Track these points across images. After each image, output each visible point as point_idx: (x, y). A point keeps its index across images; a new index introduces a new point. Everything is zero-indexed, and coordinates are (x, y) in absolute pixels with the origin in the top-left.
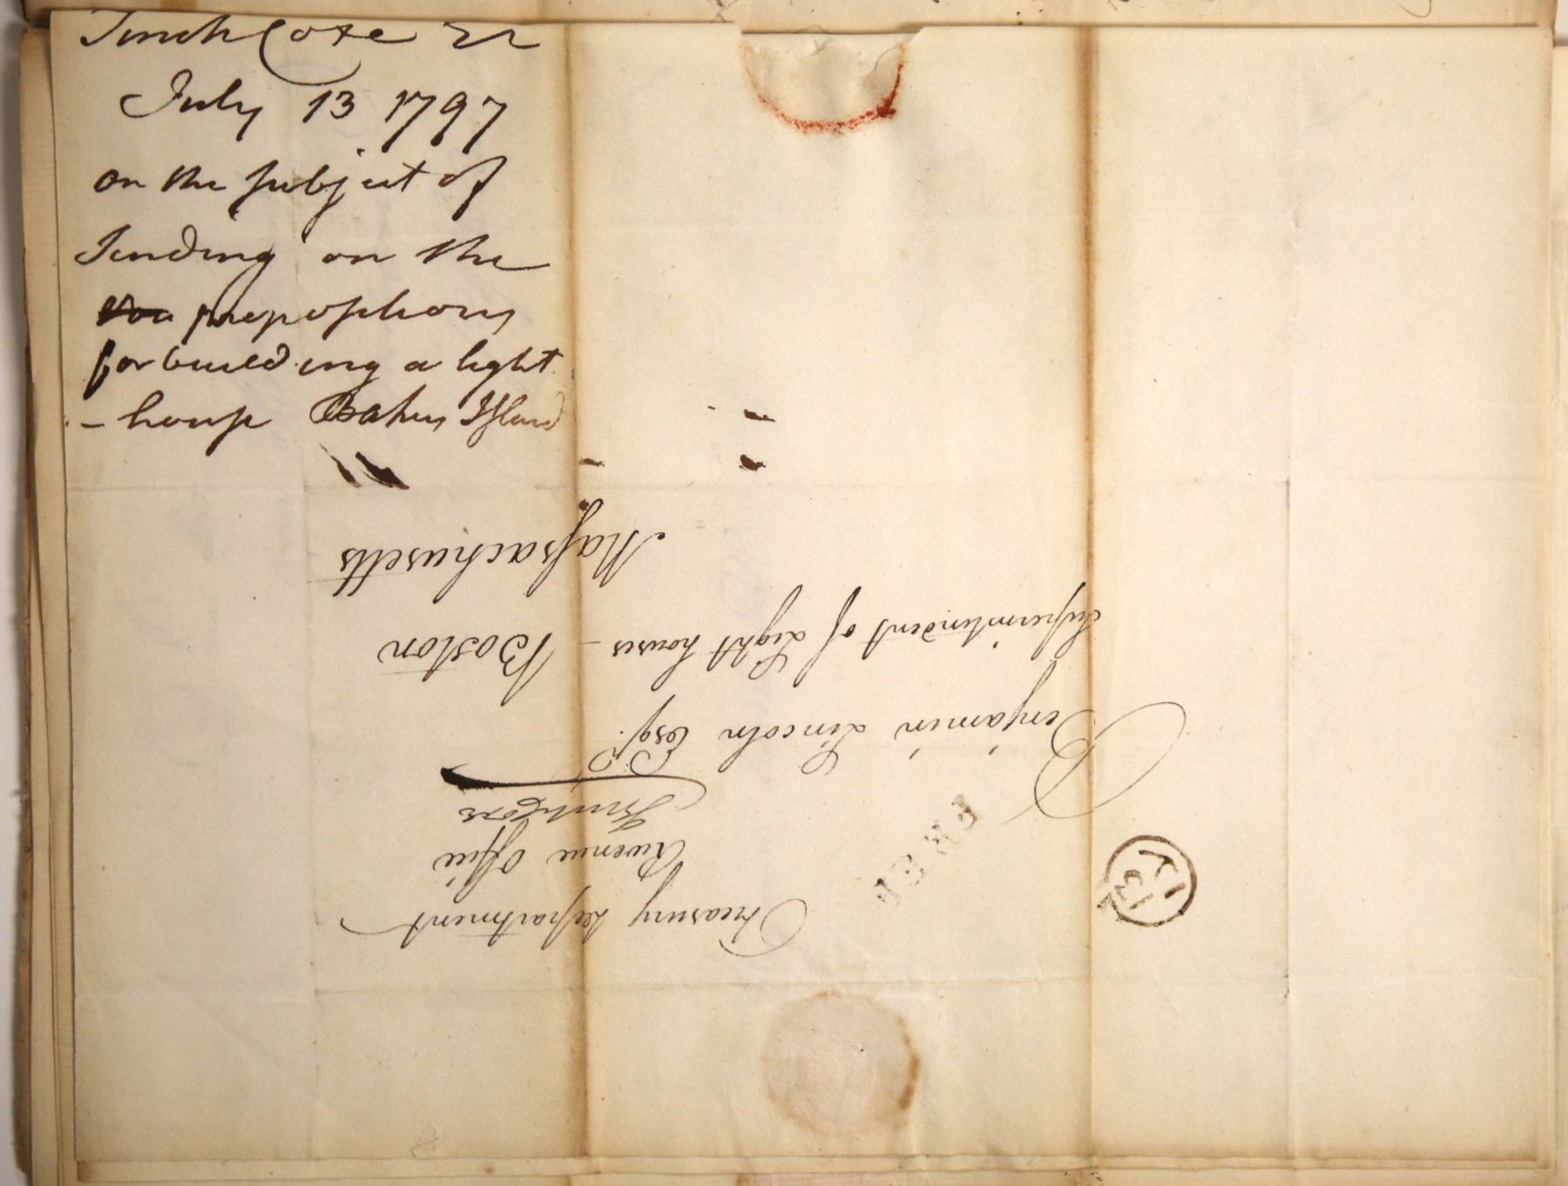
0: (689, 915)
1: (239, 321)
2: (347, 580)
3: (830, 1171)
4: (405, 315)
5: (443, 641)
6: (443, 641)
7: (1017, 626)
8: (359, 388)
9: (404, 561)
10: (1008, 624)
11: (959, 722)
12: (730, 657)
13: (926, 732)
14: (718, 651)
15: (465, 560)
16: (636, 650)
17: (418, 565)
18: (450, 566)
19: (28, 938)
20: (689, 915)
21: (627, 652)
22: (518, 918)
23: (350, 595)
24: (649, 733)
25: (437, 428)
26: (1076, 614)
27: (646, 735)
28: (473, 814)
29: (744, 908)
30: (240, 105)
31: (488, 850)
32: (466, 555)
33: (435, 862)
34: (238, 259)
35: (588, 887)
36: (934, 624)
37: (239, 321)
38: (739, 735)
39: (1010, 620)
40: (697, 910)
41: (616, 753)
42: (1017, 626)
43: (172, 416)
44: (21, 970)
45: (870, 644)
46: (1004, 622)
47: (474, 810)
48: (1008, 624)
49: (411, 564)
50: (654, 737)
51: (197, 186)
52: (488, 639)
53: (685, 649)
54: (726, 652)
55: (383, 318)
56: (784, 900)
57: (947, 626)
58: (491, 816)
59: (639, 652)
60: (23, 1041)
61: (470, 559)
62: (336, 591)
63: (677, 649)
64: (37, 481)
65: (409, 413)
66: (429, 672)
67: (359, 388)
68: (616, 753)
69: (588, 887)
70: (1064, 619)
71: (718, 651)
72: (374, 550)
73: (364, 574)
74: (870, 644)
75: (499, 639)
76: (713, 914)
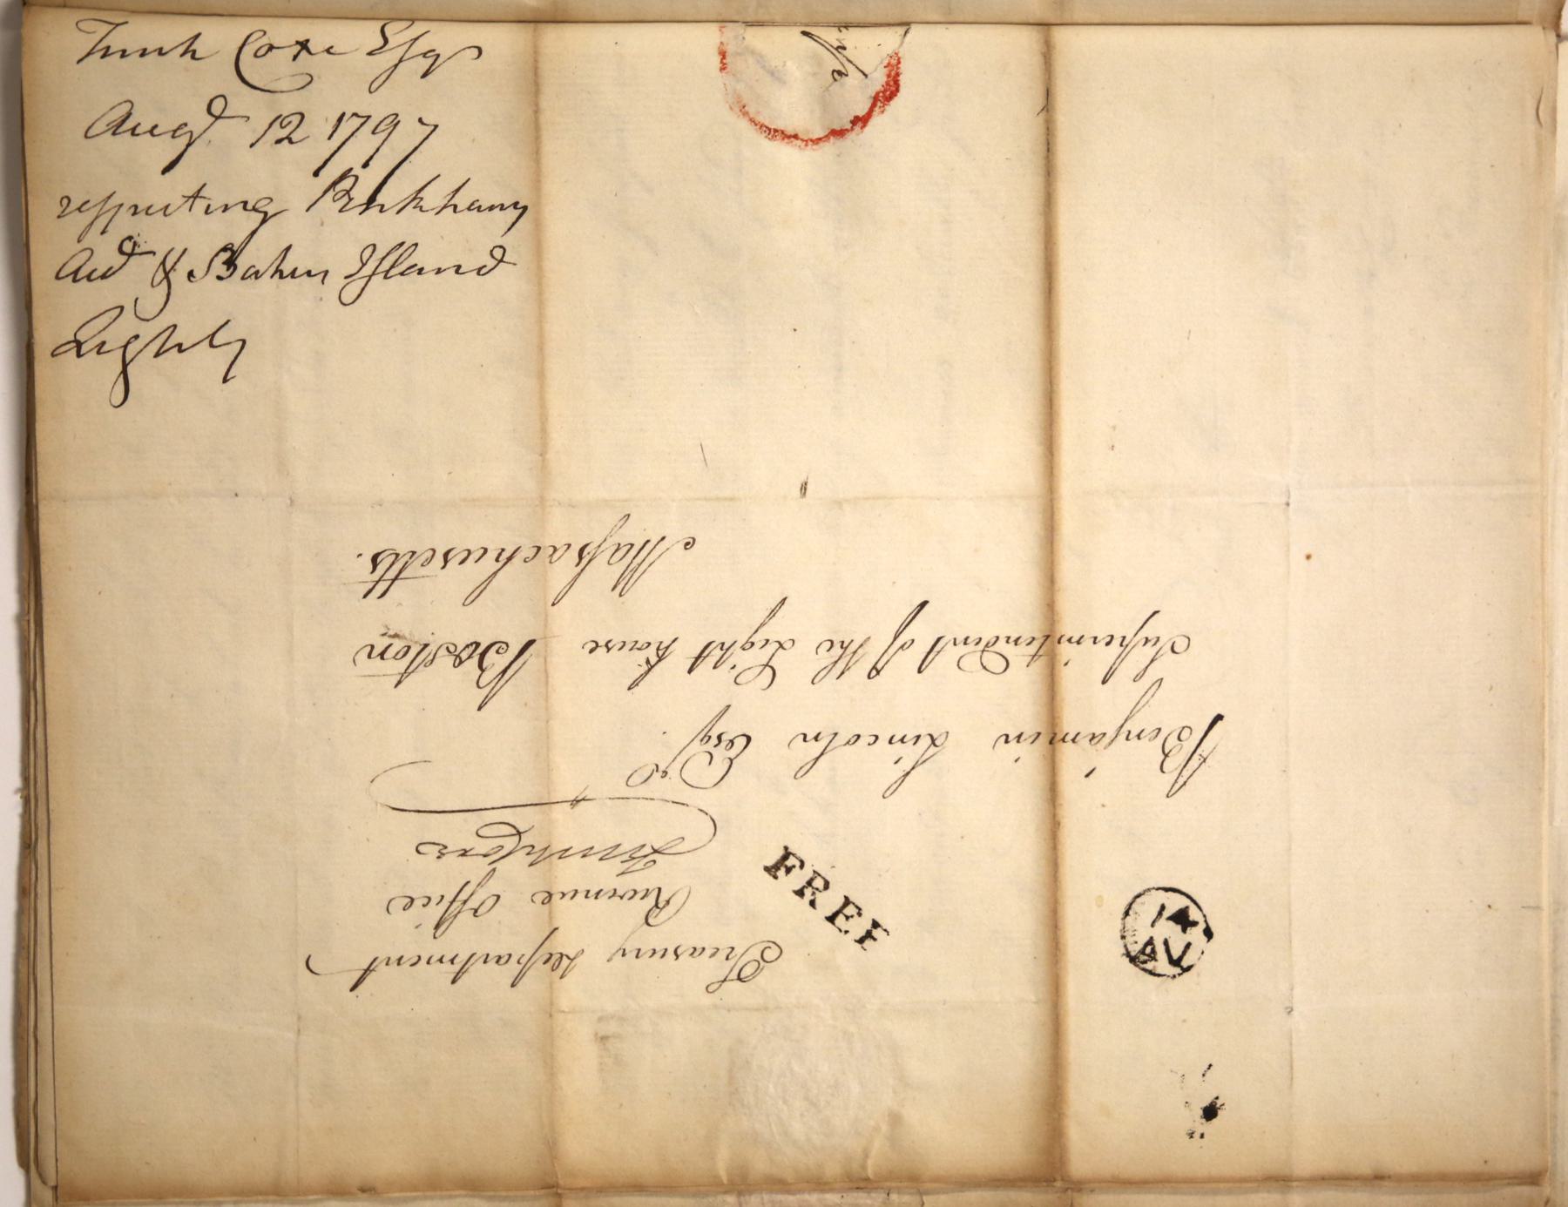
0: (670, 951)
10: (1078, 642)
12: (711, 660)
18: (489, 564)
19: (27, 934)
20: (670, 951)
24: (710, 737)
27: (707, 738)
28: (444, 851)
29: (733, 948)
30: (180, 345)
31: (1035, 655)
33: (959, 662)
35: (556, 929)
36: (998, 638)
38: (816, 739)
40: (651, 957)
44: (20, 967)
46: (1073, 640)
47: (446, 847)
48: (1078, 642)
49: (446, 561)
50: (714, 741)
56: (758, 941)
57: (1010, 641)
58: (468, 854)
60: (22, 1038)
61: (510, 559)
69: (556, 929)
73: (393, 577)
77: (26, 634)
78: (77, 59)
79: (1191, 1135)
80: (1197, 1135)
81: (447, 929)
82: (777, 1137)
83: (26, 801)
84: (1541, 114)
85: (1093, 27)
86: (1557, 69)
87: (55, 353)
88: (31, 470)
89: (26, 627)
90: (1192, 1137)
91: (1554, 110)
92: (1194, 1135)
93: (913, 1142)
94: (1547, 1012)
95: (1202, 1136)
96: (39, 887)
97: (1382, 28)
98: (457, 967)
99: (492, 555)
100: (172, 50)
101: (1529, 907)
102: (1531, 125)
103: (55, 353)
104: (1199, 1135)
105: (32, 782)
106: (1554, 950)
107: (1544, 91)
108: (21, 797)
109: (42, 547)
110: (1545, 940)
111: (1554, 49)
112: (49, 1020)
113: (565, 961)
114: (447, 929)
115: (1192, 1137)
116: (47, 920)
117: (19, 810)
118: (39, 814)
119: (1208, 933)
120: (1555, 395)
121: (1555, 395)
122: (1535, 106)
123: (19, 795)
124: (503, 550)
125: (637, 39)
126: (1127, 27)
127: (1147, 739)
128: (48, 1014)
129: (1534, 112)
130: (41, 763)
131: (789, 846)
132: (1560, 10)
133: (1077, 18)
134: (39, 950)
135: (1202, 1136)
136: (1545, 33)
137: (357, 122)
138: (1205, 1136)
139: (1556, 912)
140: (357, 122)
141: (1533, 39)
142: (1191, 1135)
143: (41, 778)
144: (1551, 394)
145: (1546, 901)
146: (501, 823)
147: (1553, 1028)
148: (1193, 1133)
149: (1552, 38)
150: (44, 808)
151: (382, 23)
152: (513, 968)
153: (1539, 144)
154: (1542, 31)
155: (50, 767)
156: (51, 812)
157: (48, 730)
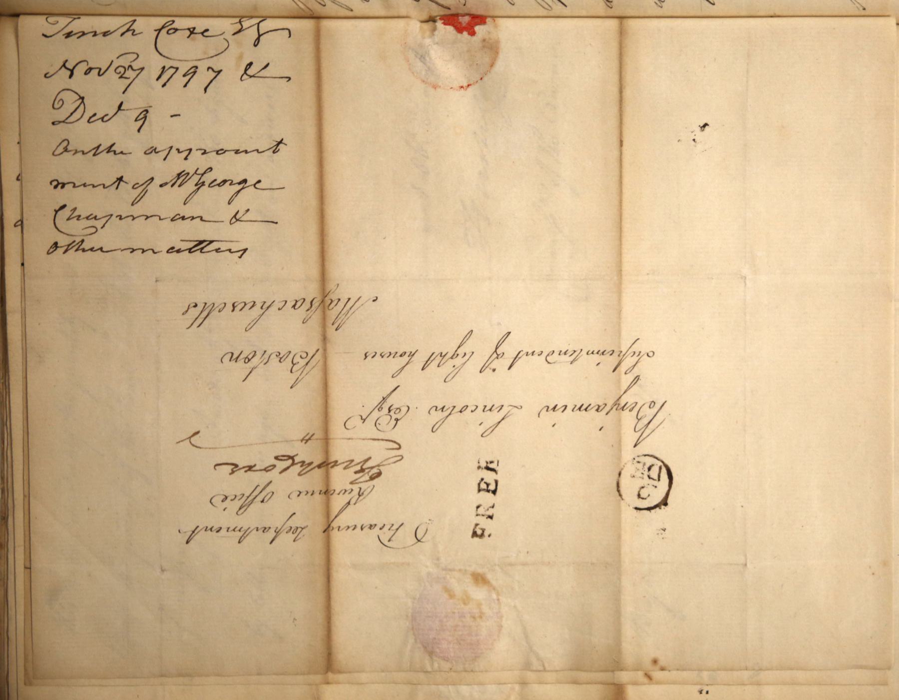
1: (119, 154)
4: (97, 218)
5: (291, 302)
6: (291, 302)
7: (593, 412)
8: (60, 122)
9: (230, 307)
13: (558, 413)
15: (365, 527)
17: (237, 309)
18: (257, 311)
22: (318, 301)
25: (508, 412)
32: (395, 527)
34: (48, 35)
37: (119, 154)
39: (587, 408)
42: (593, 412)
51: (84, 250)
52: (299, 307)
54: (519, 358)
55: (190, 252)
62: (638, 341)
65: (406, 358)
67: (60, 122)
70: (592, 408)
72: (210, 303)
76: (267, 529)
79: (701, 692)
80: (704, 692)
81: (144, 195)
87: (17, 225)
90: (701, 693)
93: (534, 697)
95: (707, 692)
98: (241, 534)
99: (259, 305)
100: (265, 33)
103: (17, 225)
109: (9, 341)
113: (299, 530)
114: (144, 195)
115: (701, 693)
124: (265, 302)
127: (537, 355)
128: (14, 621)
130: (10, 470)
131: (179, 148)
135: (707, 692)
137: (173, 70)
138: (709, 692)
140: (173, 70)
142: (701, 692)
146: (290, 517)
148: (702, 691)
151: (240, 18)
152: (271, 534)
155: (14, 473)
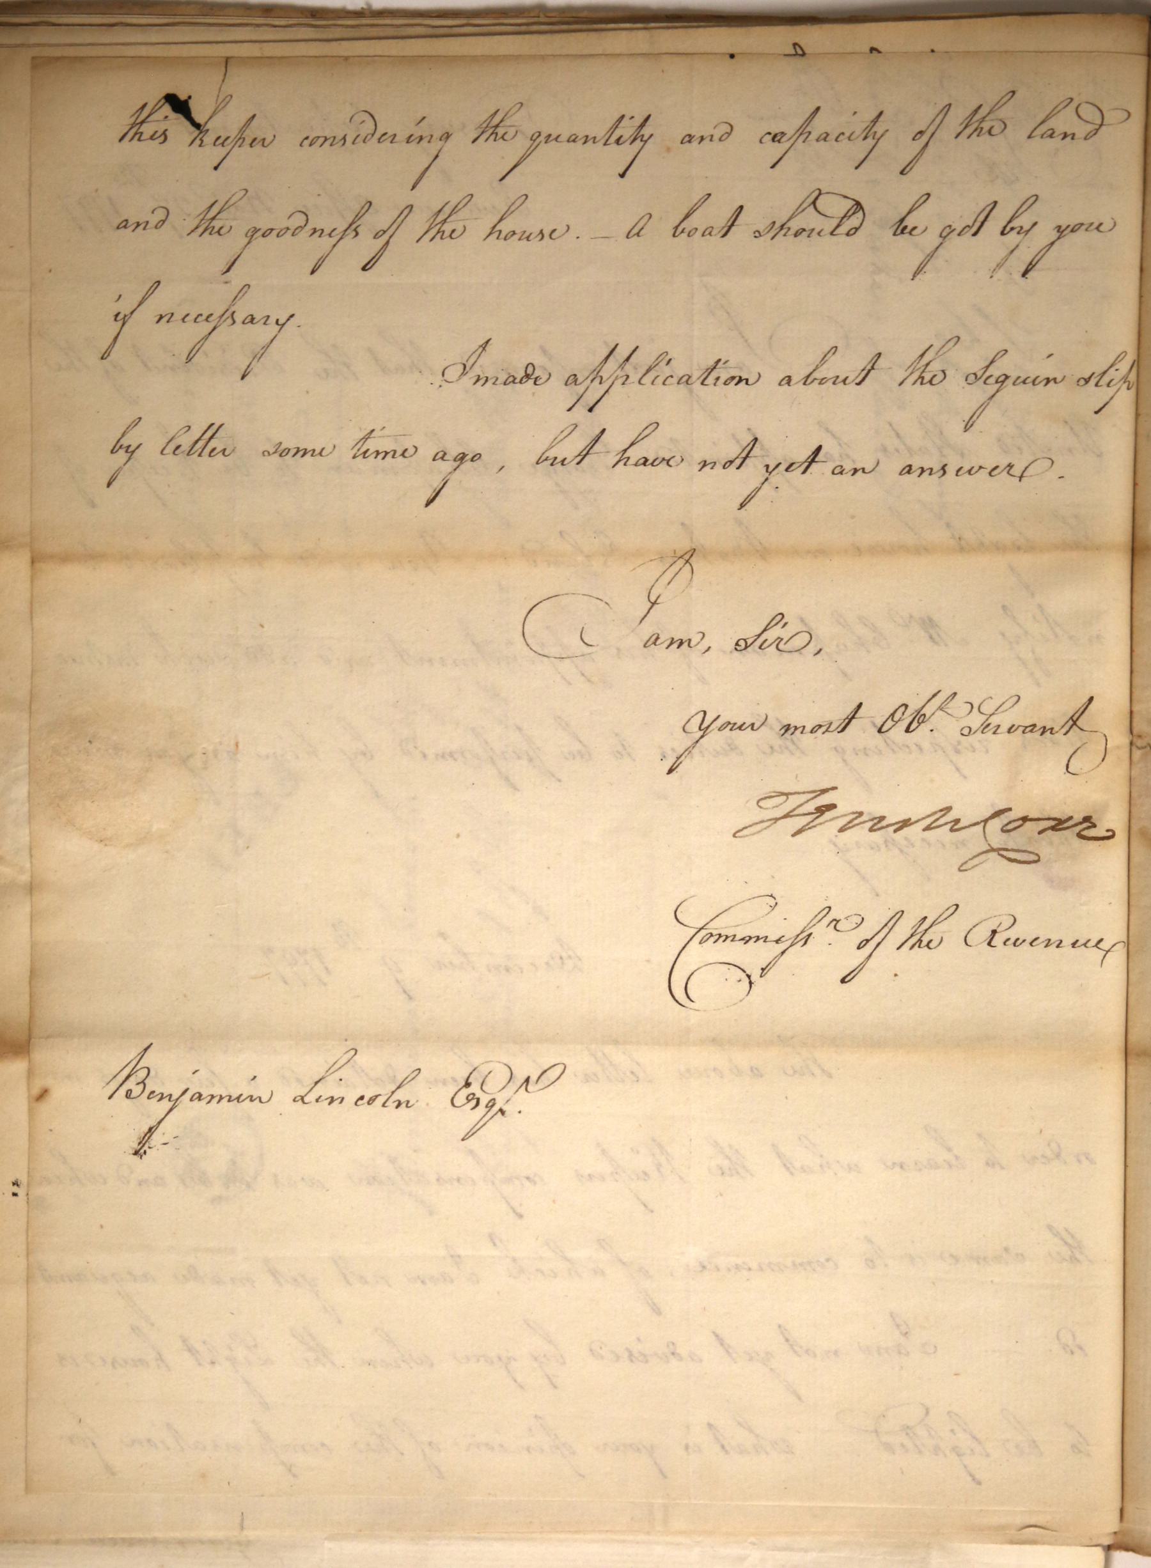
2: (211, 438)
3: (29, 673)
11: (449, 234)
14: (585, 455)
16: (546, 233)
21: (156, 132)
23: (213, 424)
26: (362, 456)
41: (441, 234)
43: (552, 133)
45: (747, 456)
53: (643, 143)
59: (167, 133)
63: (797, 228)
64: (681, 32)
66: (369, 437)
68: (441, 234)
71: (585, 455)
74: (747, 456)
75: (110, 450)
77: (526, 15)
78: (863, 707)
80: (15, 1189)
82: (14, 770)
83: (359, 14)
84: (1032, 1529)
85: (1123, 1158)
86: (1076, 1545)
88: (703, 21)
89: (532, 15)
90: (14, 1184)
91: (1033, 1542)
92: (15, 1186)
93: (9, 906)
94: (140, 1535)
95: (15, 1194)
96: (186, 28)
97: (1120, 1405)
101: (243, 1520)
102: (1019, 1520)
104: (16, 1192)
105: (376, 21)
106: (202, 1542)
107: (1054, 1533)
108: (362, 8)
110: (211, 1534)
111: (1094, 1543)
112: (132, 40)
115: (14, 1184)
116: (231, 38)
117: (351, 6)
118: (339, 29)
119: (217, 1200)
120: (754, 1544)
121: (754, 1544)
122: (1039, 1524)
123: (365, 7)
125: (1116, 627)
126: (1124, 1099)
129: (1032, 1523)
132: (1133, 1550)
133: (1130, 1068)
134: (294, 29)
135: (15, 1194)
136: (1110, 1534)
138: (15, 1197)
139: (239, 1543)
141: (1107, 1524)
142: (15, 1184)
143: (374, 32)
144: (752, 1539)
145: (250, 1534)
147: (124, 1540)
148: (18, 1185)
149: (1107, 1541)
150: (346, 36)
153: (1000, 1528)
154: (1113, 1531)
156: (338, 42)
157: (510, 37)
